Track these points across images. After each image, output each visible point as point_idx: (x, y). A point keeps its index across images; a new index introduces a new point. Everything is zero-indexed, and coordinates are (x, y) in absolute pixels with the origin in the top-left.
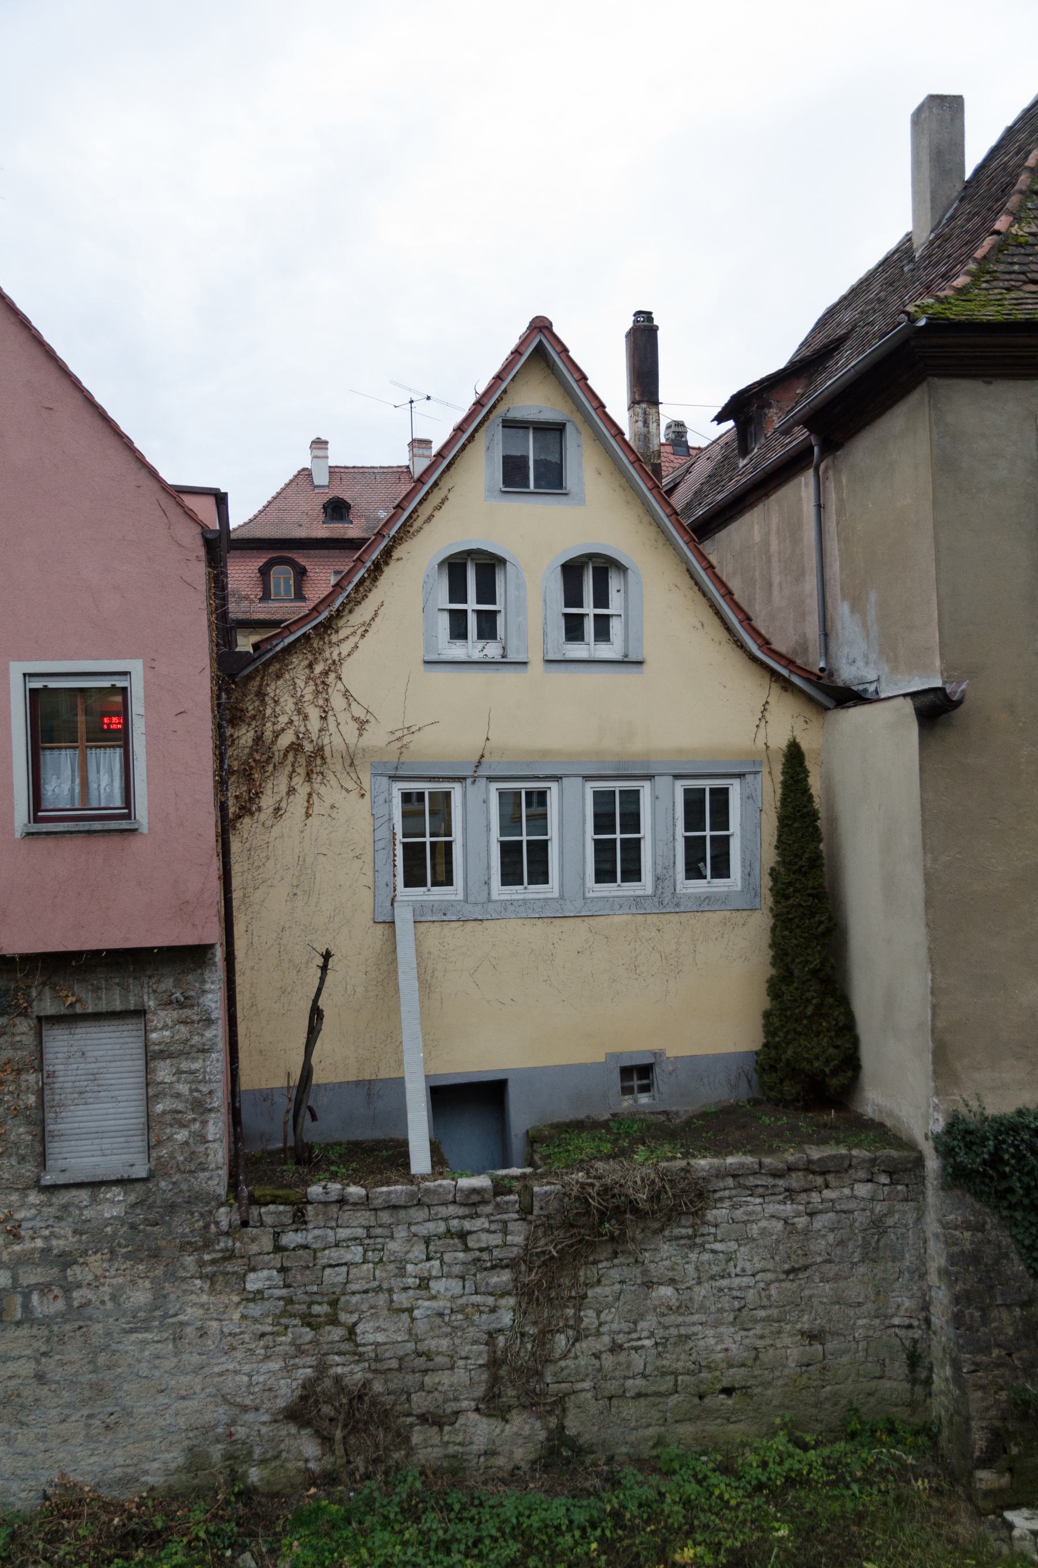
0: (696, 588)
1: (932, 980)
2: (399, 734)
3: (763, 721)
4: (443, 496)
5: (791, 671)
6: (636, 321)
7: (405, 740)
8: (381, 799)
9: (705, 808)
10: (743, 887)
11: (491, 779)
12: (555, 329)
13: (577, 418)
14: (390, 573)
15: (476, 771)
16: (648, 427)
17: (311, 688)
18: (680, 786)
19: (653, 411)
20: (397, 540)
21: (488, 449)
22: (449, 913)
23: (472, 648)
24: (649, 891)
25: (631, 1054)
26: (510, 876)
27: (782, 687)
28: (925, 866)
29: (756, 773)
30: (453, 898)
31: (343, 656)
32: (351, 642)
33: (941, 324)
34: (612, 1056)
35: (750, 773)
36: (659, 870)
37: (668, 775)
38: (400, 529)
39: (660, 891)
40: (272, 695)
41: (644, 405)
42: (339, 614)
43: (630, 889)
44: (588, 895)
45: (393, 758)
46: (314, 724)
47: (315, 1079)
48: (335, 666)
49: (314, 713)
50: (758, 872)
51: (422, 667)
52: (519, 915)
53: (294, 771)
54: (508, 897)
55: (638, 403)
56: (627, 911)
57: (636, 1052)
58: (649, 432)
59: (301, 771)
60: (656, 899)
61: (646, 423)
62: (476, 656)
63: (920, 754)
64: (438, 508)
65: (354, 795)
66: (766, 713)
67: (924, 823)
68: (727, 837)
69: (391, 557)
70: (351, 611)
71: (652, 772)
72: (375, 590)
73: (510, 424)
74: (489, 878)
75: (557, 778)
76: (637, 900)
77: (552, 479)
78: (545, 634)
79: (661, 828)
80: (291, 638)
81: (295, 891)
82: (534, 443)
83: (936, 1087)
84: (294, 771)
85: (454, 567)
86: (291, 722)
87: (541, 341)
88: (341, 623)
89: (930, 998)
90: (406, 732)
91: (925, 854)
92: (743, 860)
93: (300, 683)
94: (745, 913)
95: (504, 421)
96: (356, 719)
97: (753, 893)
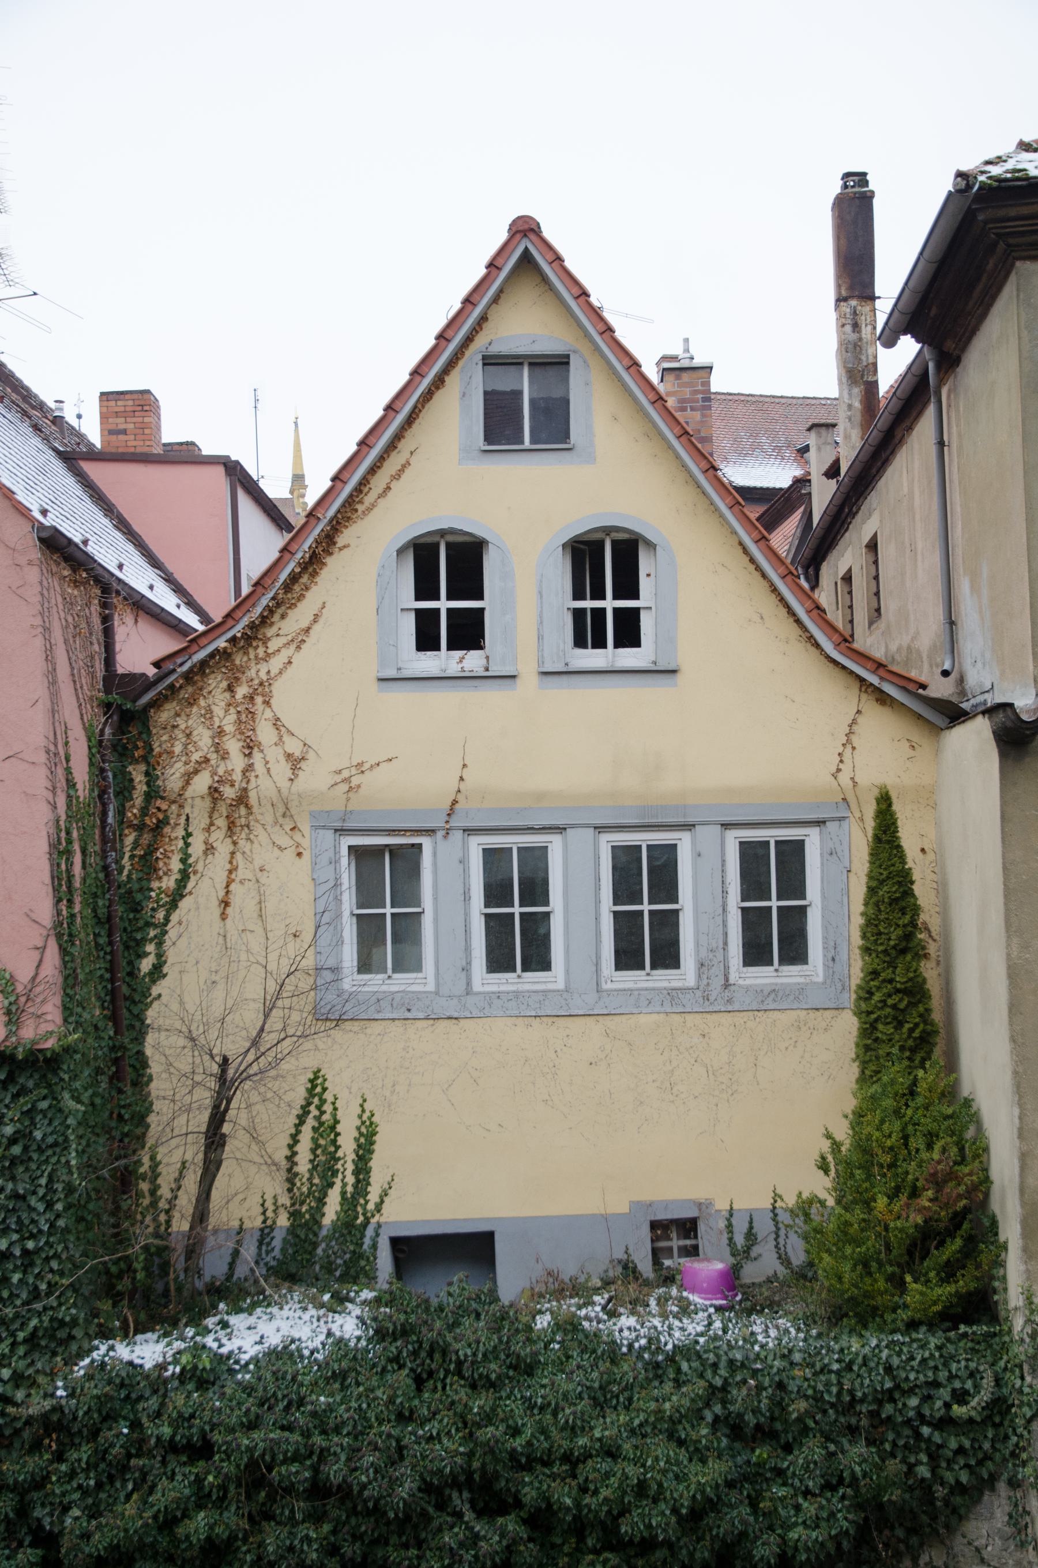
0: (752, 567)
1: (1020, 1118)
2: (346, 774)
3: (849, 747)
4: (403, 462)
5: (882, 678)
6: (845, 186)
7: (355, 781)
8: (324, 859)
9: (772, 870)
10: (826, 977)
11: (469, 831)
12: (547, 233)
13: (584, 348)
14: (334, 565)
15: (452, 819)
16: (859, 332)
17: (232, 717)
18: (732, 839)
19: (867, 309)
20: (337, 525)
21: (464, 395)
22: (413, 1009)
23: (444, 660)
24: (561, 985)
25: (666, 1205)
26: (499, 960)
27: (877, 700)
28: (1008, 955)
29: (841, 819)
30: (551, 986)
31: (272, 674)
32: (285, 654)
33: (1009, 187)
34: (636, 1205)
35: (833, 819)
36: (704, 953)
37: (715, 823)
38: (343, 505)
39: (705, 982)
40: (183, 727)
41: (854, 303)
42: (265, 620)
43: (664, 978)
44: (605, 987)
45: (339, 806)
46: (237, 762)
47: (213, 1221)
48: (262, 690)
49: (233, 746)
50: (846, 957)
51: (375, 685)
52: (508, 1013)
53: (212, 824)
54: (495, 988)
55: (845, 299)
56: (658, 1009)
57: (673, 1202)
58: (860, 339)
59: (221, 822)
60: (699, 993)
61: (856, 326)
62: (454, 669)
63: (1002, 797)
64: (397, 476)
65: (290, 853)
66: (852, 737)
67: (1008, 893)
68: (676, 912)
69: (335, 543)
70: (283, 617)
71: (690, 819)
72: (314, 589)
73: (490, 361)
74: (469, 963)
75: (560, 829)
76: (673, 994)
77: (554, 427)
78: (540, 638)
79: (708, 900)
80: (202, 655)
81: (214, 978)
82: (531, 383)
83: (1027, 1271)
84: (212, 824)
85: (423, 553)
86: (207, 760)
87: (526, 249)
88: (270, 632)
89: (1017, 1142)
90: (354, 771)
91: (1009, 937)
92: (825, 939)
93: (218, 711)
94: (828, 1013)
95: (484, 358)
96: (289, 756)
97: (839, 986)
